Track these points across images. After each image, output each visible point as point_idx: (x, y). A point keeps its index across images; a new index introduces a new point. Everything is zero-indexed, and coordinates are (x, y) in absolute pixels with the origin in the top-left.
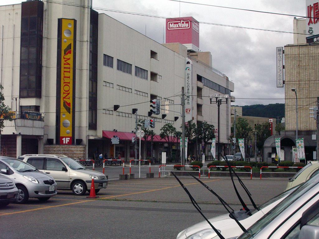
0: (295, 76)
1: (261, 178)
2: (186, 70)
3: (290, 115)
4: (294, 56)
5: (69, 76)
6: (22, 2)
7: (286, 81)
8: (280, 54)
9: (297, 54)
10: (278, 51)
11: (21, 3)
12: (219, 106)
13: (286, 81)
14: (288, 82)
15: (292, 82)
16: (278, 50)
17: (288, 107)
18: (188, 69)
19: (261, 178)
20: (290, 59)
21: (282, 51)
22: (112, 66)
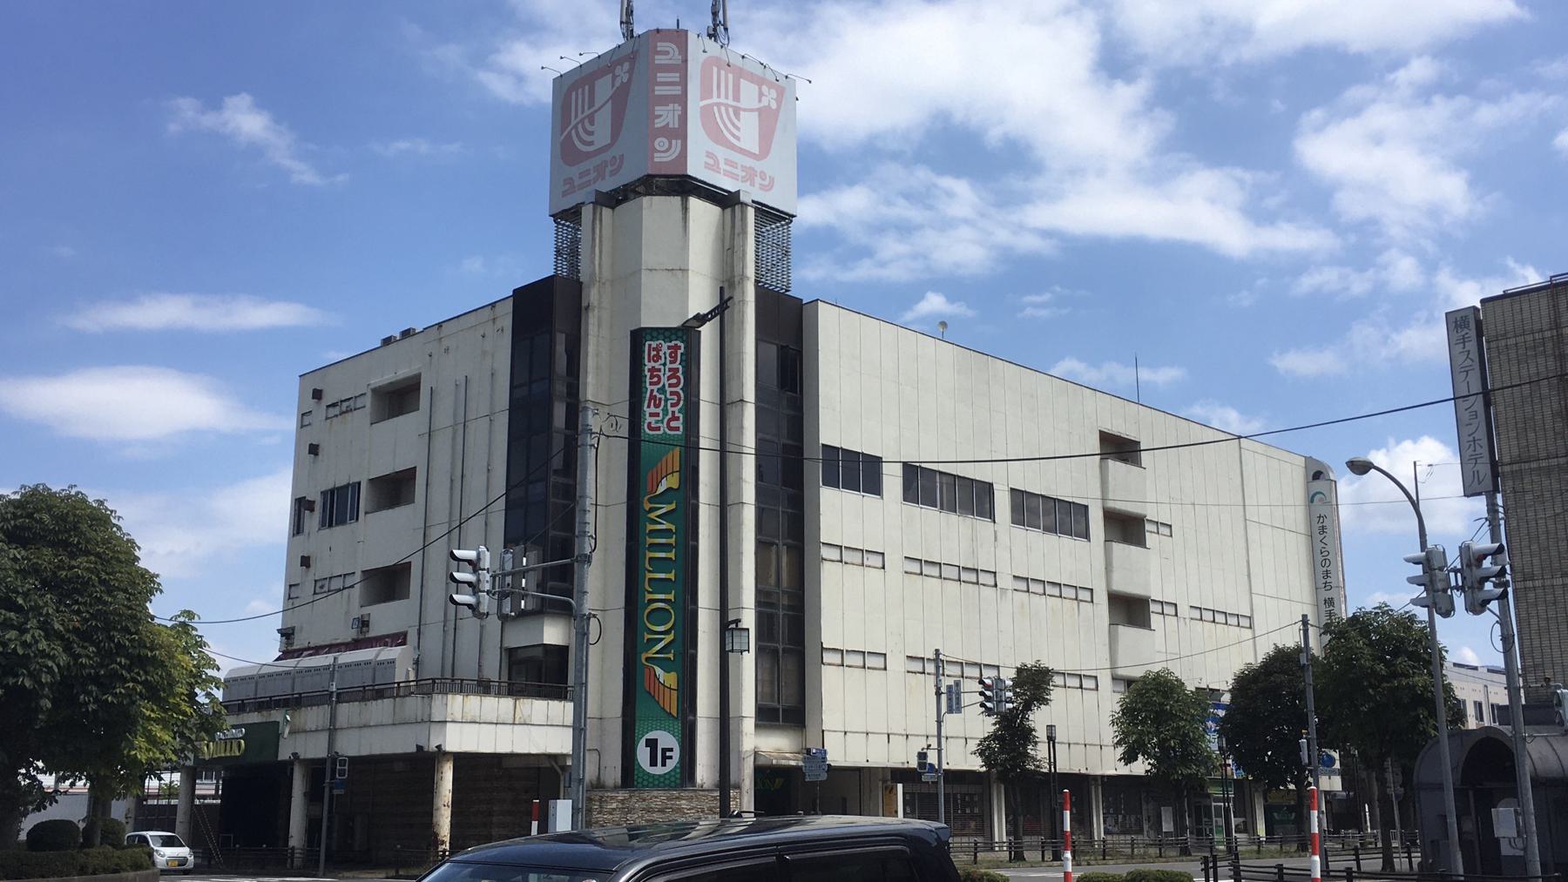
0: (1550, 434)
1: (397, 872)
2: (1312, 501)
3: (1543, 624)
4: (1530, 338)
5: (368, 515)
6: (514, 291)
7: (1506, 459)
8: (1464, 340)
9: (1545, 327)
10: (1456, 327)
11: (511, 294)
12: (825, 560)
13: (1506, 459)
14: (1515, 467)
15: (1534, 465)
16: (1456, 322)
17: (1529, 584)
18: (1321, 500)
19: (397, 872)
20: (1513, 355)
21: (1472, 325)
22: (1086, 535)
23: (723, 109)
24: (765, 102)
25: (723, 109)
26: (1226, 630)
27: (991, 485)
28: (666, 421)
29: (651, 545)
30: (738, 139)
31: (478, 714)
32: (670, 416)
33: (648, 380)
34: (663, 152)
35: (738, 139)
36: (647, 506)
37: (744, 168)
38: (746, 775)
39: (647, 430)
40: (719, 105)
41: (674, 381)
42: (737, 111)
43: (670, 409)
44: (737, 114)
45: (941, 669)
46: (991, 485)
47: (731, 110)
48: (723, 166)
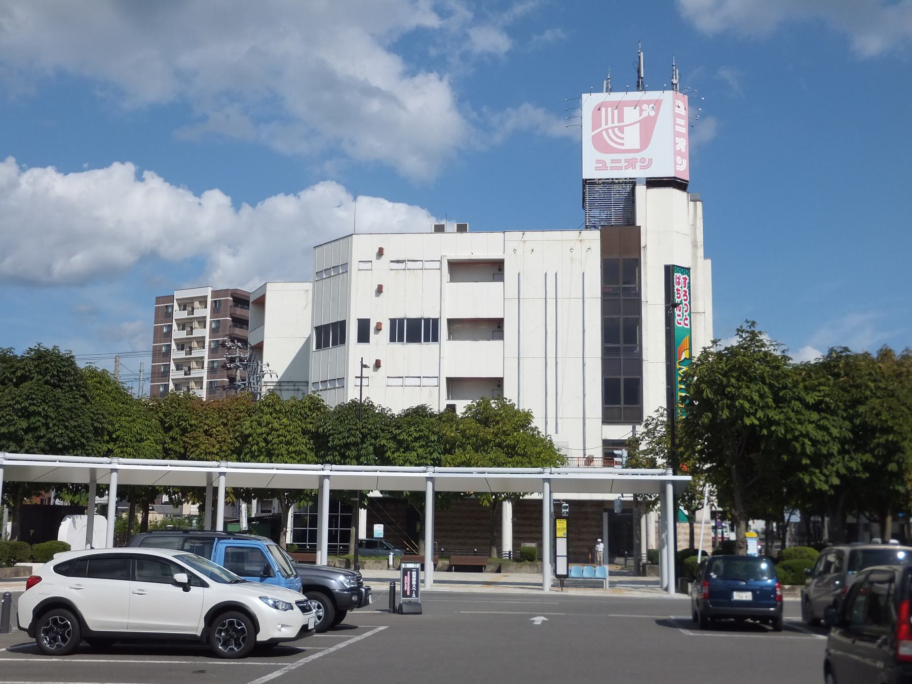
23: (610, 131)
24: (645, 114)
25: (610, 131)
26: (149, 353)
27: (156, 298)
28: (683, 319)
29: (680, 388)
30: (623, 144)
31: (359, 398)
32: (684, 317)
33: (676, 296)
34: (647, 165)
35: (623, 144)
36: (678, 366)
37: (626, 161)
38: (735, 531)
39: (677, 325)
40: (607, 130)
41: (685, 298)
42: (621, 129)
43: (685, 313)
44: (622, 131)
45: (287, 384)
46: (156, 298)
47: (616, 130)
48: (609, 164)
